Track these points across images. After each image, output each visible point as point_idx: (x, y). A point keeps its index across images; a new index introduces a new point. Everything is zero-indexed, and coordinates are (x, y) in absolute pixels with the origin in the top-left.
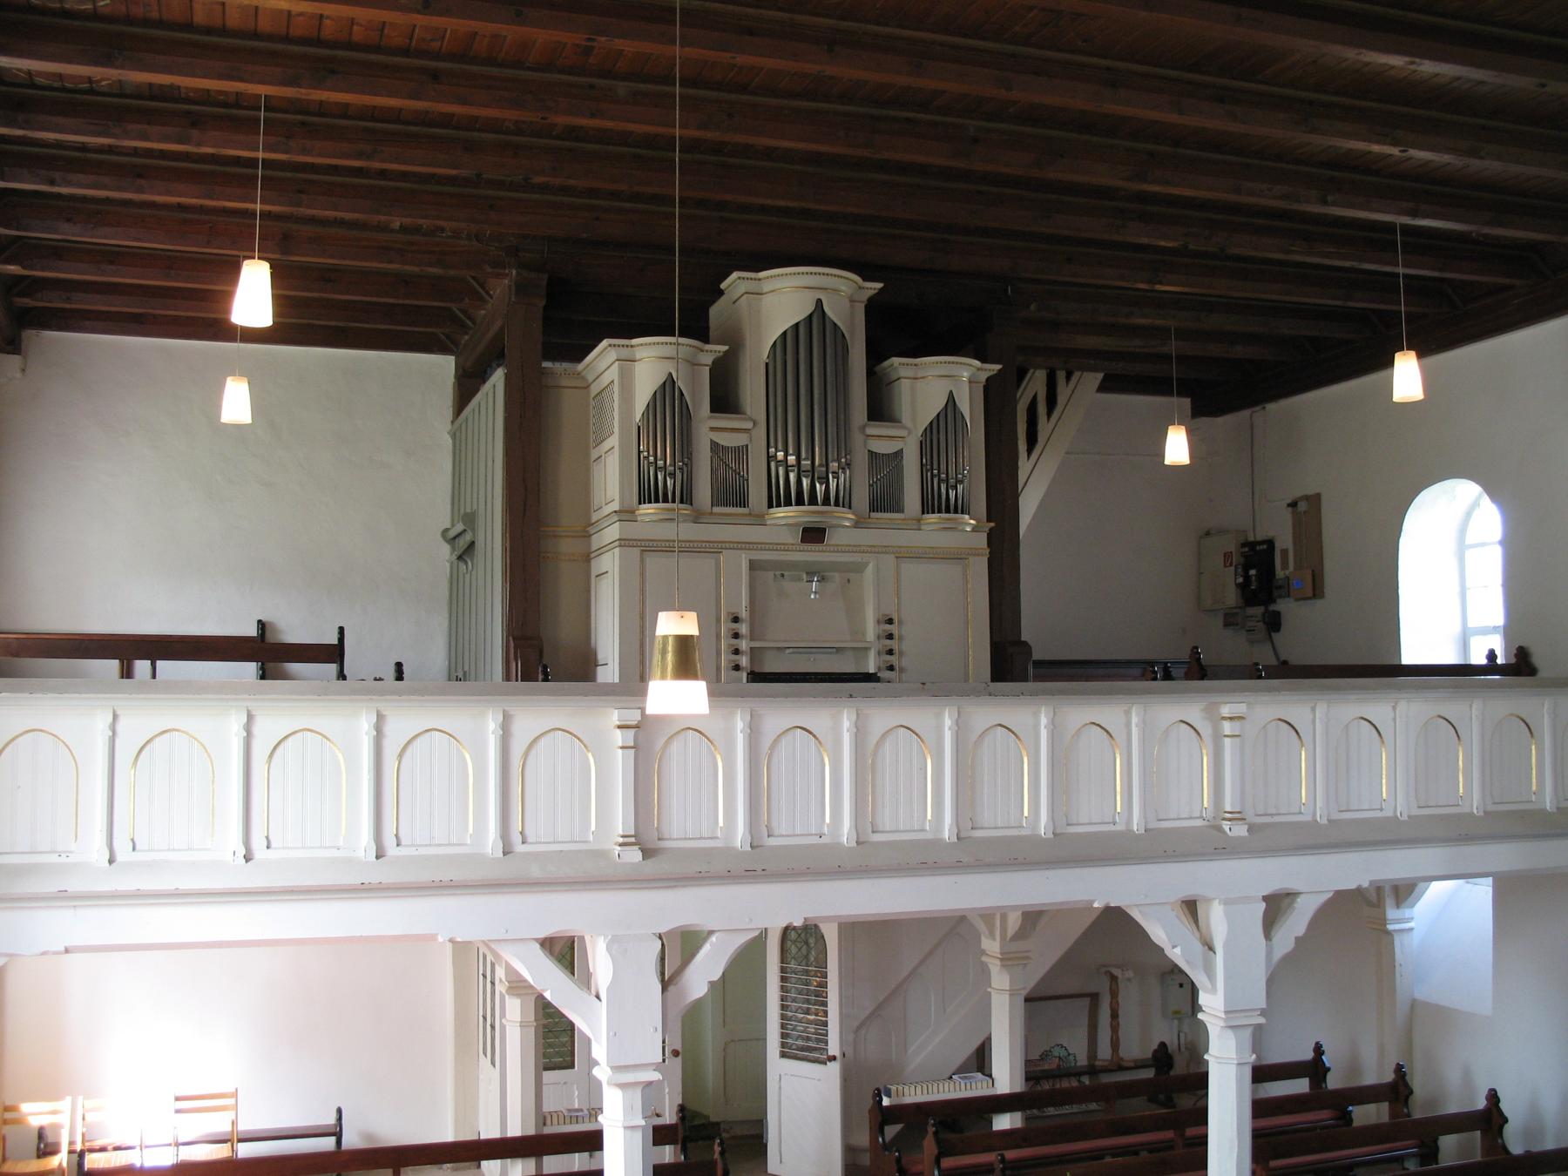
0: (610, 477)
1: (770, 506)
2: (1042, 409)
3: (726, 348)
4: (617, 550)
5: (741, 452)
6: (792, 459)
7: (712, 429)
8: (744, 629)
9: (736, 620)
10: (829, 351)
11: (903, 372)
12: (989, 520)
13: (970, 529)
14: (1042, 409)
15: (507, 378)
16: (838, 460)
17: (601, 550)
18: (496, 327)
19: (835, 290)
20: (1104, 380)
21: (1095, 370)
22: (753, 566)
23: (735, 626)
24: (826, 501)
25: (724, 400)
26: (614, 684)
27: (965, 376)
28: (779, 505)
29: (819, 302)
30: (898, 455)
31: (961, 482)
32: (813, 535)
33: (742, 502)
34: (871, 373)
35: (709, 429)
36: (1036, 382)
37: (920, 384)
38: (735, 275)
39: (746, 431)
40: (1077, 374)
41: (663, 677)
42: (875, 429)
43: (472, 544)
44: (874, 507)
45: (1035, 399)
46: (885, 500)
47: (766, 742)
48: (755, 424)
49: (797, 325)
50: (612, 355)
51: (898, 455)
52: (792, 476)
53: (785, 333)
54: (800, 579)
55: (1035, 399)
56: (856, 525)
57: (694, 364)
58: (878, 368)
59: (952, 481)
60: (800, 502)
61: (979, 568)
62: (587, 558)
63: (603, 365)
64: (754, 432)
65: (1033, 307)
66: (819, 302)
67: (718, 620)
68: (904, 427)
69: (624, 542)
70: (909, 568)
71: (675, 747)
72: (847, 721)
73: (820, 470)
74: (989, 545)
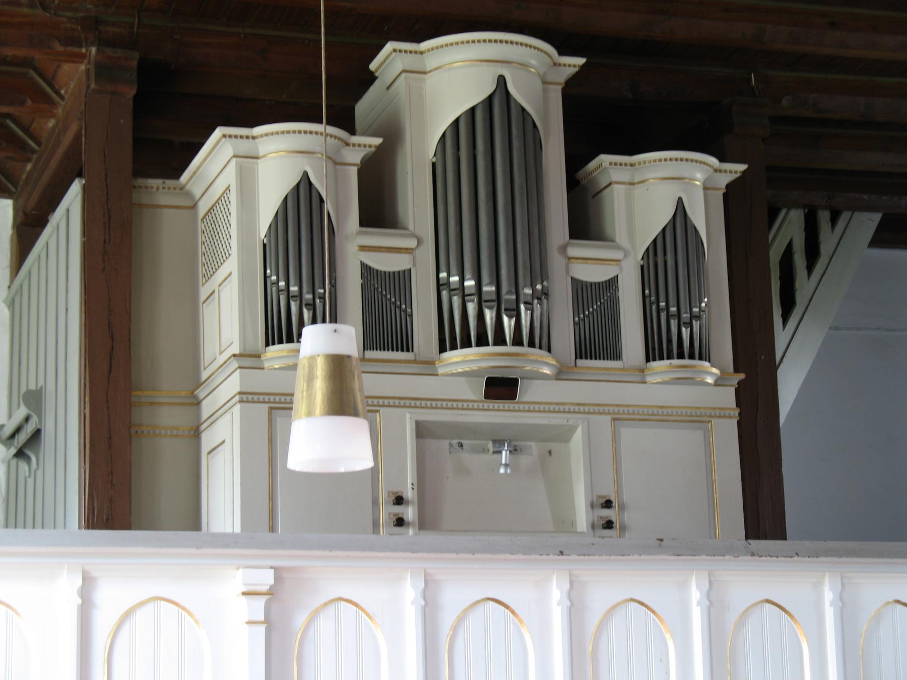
0: (227, 309)
1: (442, 349)
2: (800, 261)
3: (378, 141)
4: (238, 406)
5: (402, 280)
6: (470, 283)
7: (363, 248)
8: (410, 513)
9: (399, 500)
10: (516, 144)
11: (616, 175)
12: (737, 370)
13: (710, 383)
14: (800, 261)
15: (85, 189)
16: (533, 286)
17: (214, 418)
18: (67, 140)
19: (524, 66)
20: (881, 228)
21: (869, 208)
22: (422, 431)
23: (398, 509)
24: (517, 341)
25: (378, 211)
26: (233, 535)
27: (699, 177)
28: (454, 347)
29: (501, 81)
30: (612, 283)
31: (698, 317)
32: (501, 388)
33: (405, 344)
34: (573, 183)
35: (358, 250)
36: (790, 227)
37: (639, 191)
38: (390, 46)
39: (409, 249)
40: (845, 216)
41: (310, 414)
42: (580, 249)
43: (37, 434)
44: (584, 350)
45: (790, 246)
46: (597, 341)
47: (447, 620)
48: (420, 242)
49: (473, 110)
50: (227, 150)
51: (612, 283)
52: (471, 308)
53: (457, 122)
54: (484, 450)
55: (790, 246)
56: (561, 374)
57: (336, 163)
58: (581, 174)
59: (685, 316)
60: (482, 341)
61: (726, 436)
62: (196, 434)
63: (213, 168)
64: (418, 253)
65: (785, 102)
66: (501, 81)
67: (375, 502)
68: (618, 248)
69: (246, 397)
70: (630, 434)
71: (324, 625)
72: (556, 592)
73: (508, 297)
74: (738, 404)
